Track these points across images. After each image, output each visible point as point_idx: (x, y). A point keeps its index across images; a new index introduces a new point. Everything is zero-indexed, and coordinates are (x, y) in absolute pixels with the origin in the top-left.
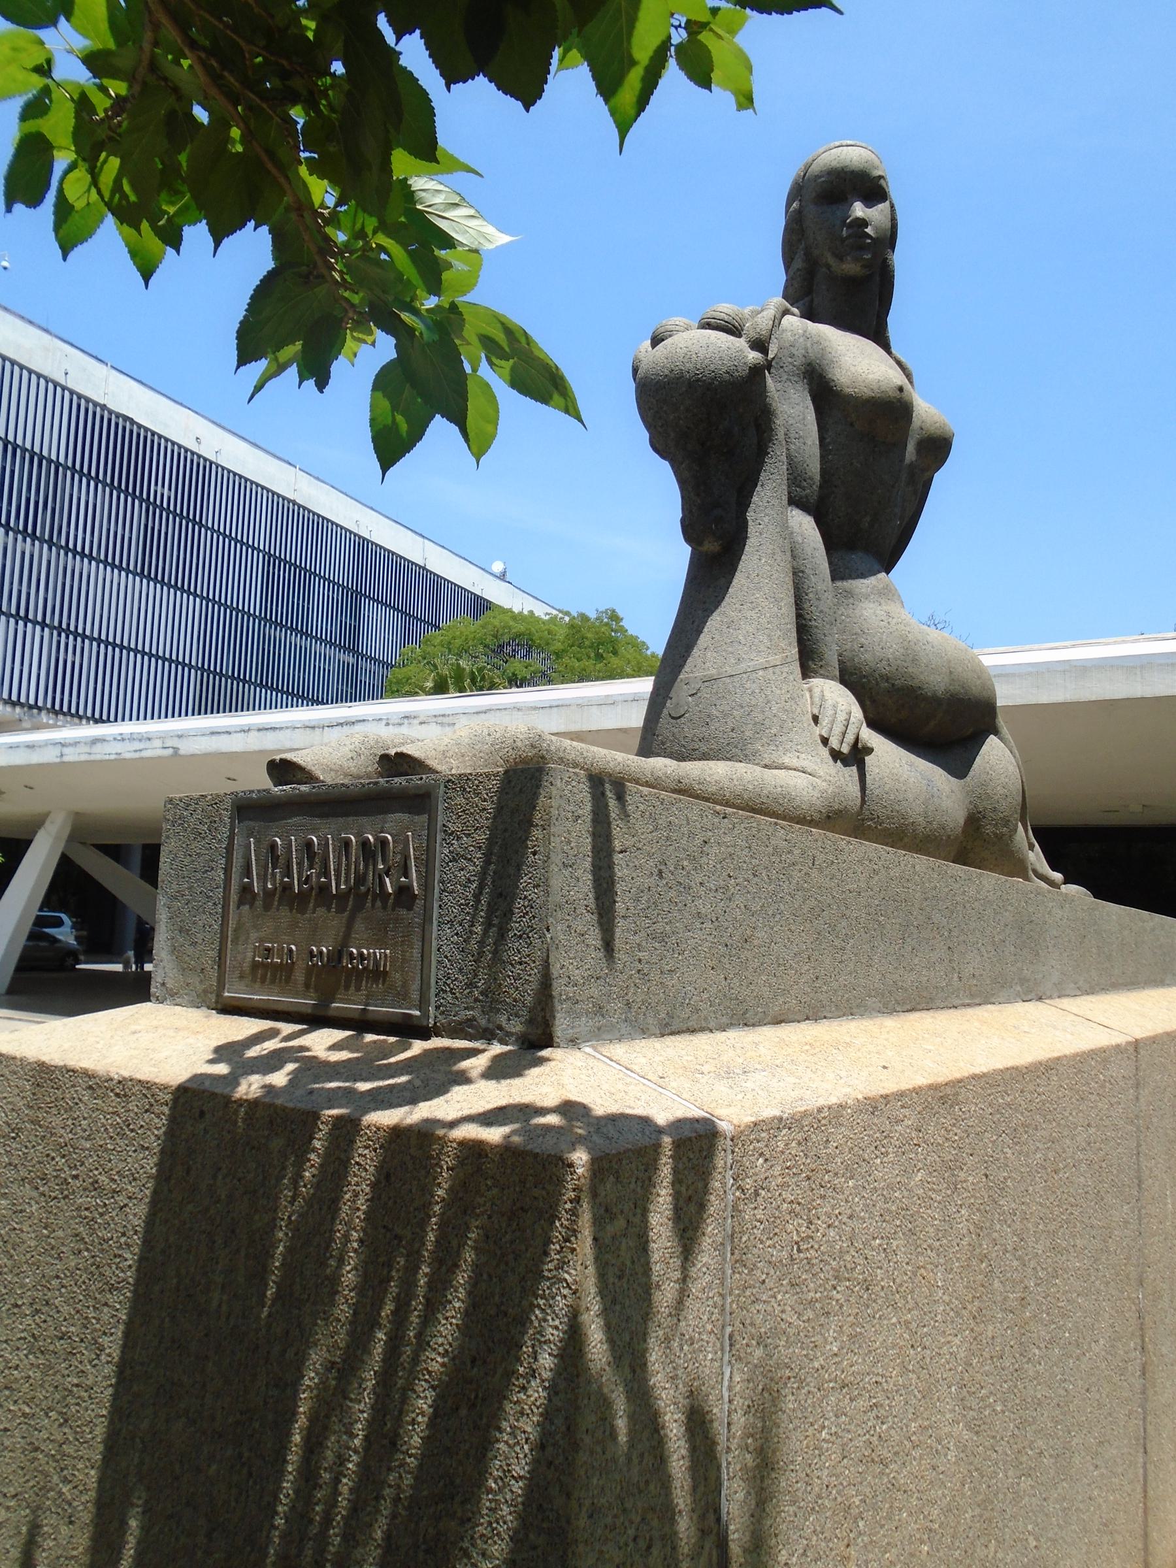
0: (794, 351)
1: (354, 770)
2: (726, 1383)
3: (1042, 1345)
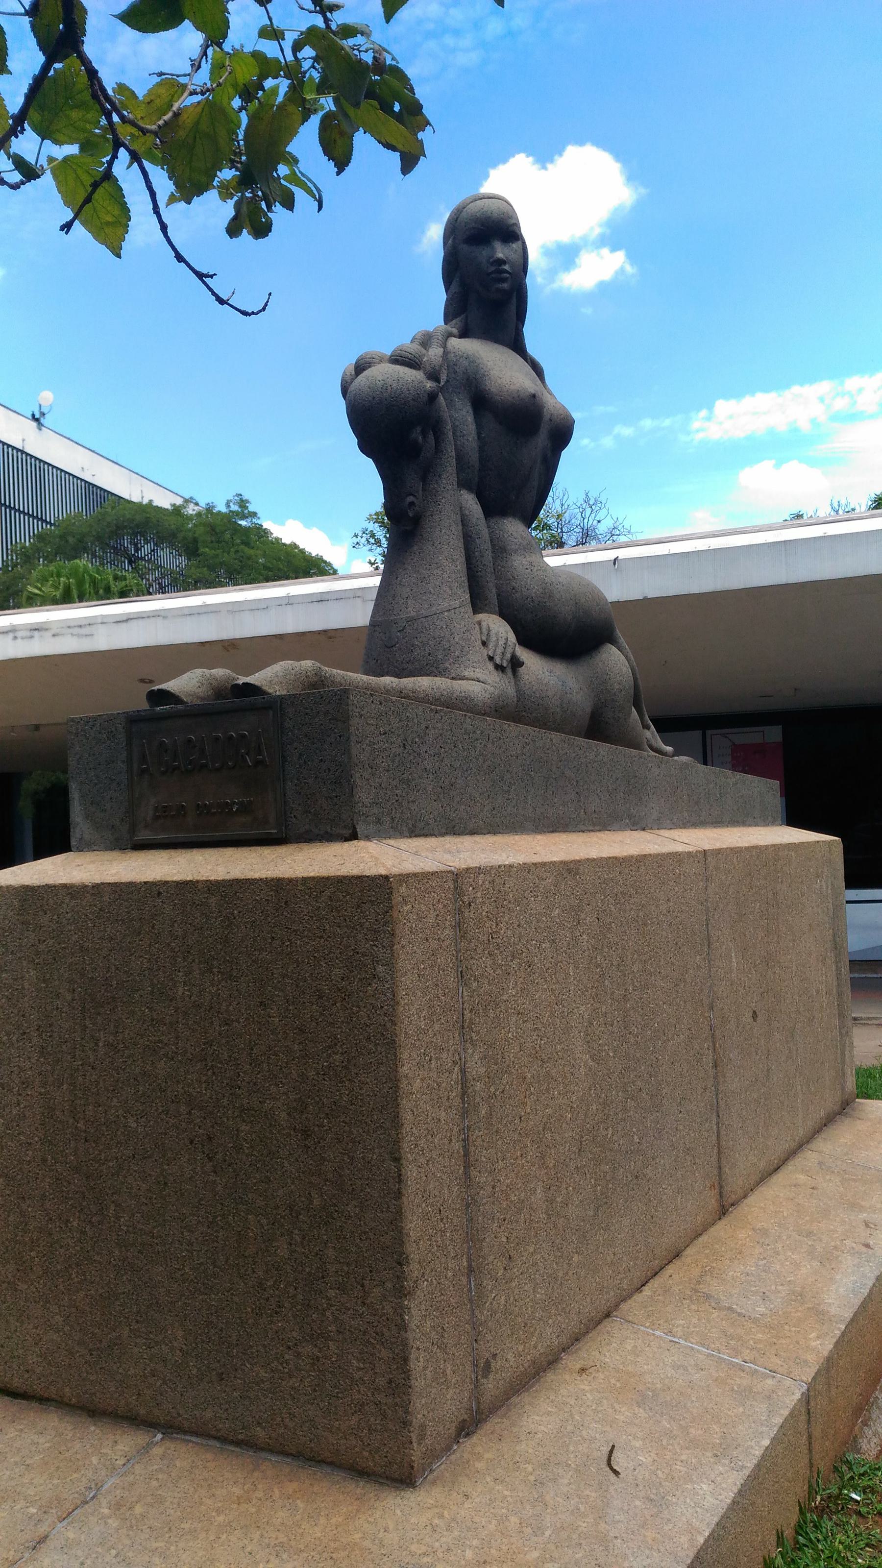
0: (456, 368)
1: (202, 695)
2: (460, 995)
3: (639, 1026)
